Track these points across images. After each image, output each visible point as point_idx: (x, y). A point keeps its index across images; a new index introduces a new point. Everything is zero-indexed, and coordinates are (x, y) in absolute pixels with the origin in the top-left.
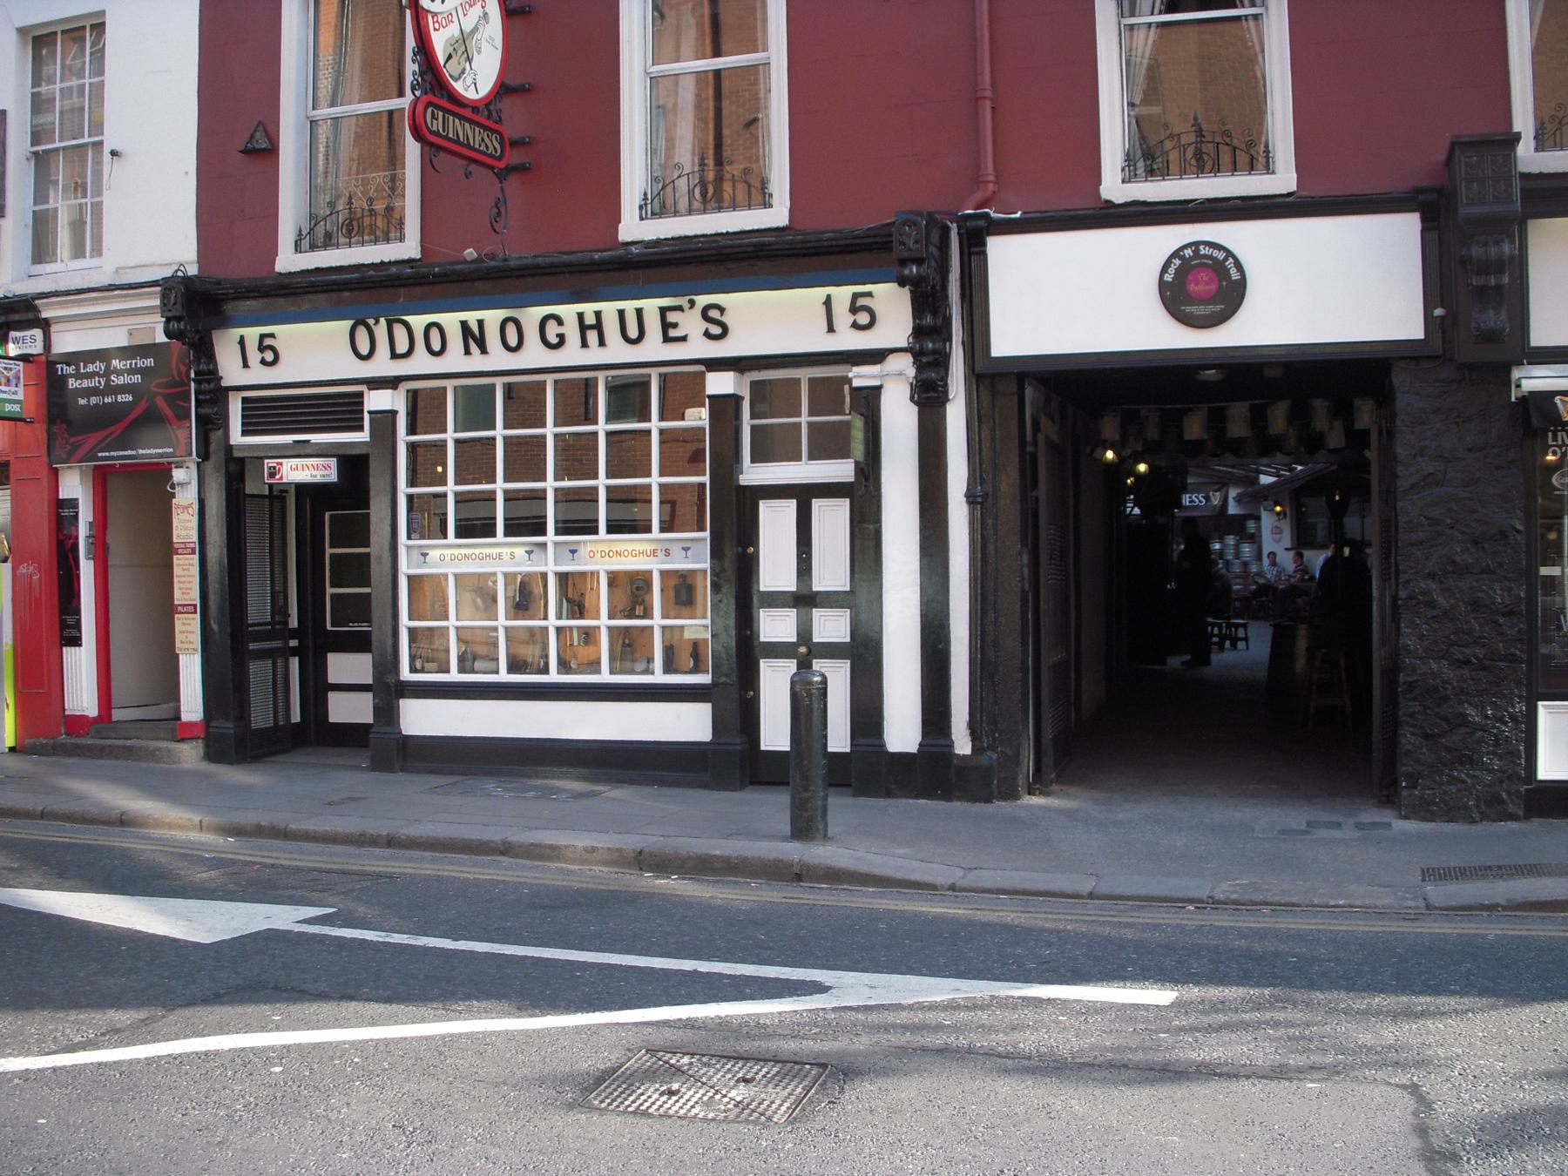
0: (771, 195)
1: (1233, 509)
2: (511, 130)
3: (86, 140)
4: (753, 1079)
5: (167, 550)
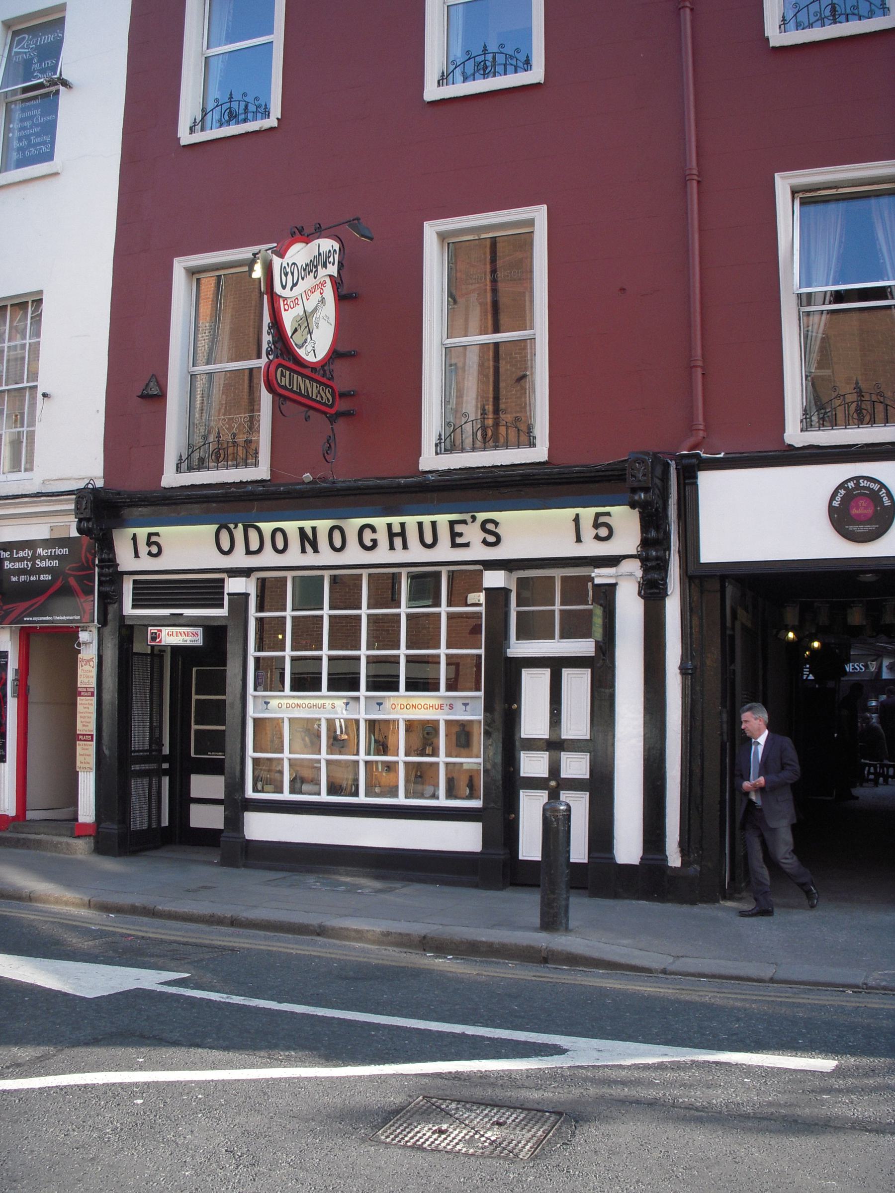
0: (535, 438)
1: (886, 675)
2: (341, 385)
3: (25, 384)
4: (505, 1123)
5: (73, 692)
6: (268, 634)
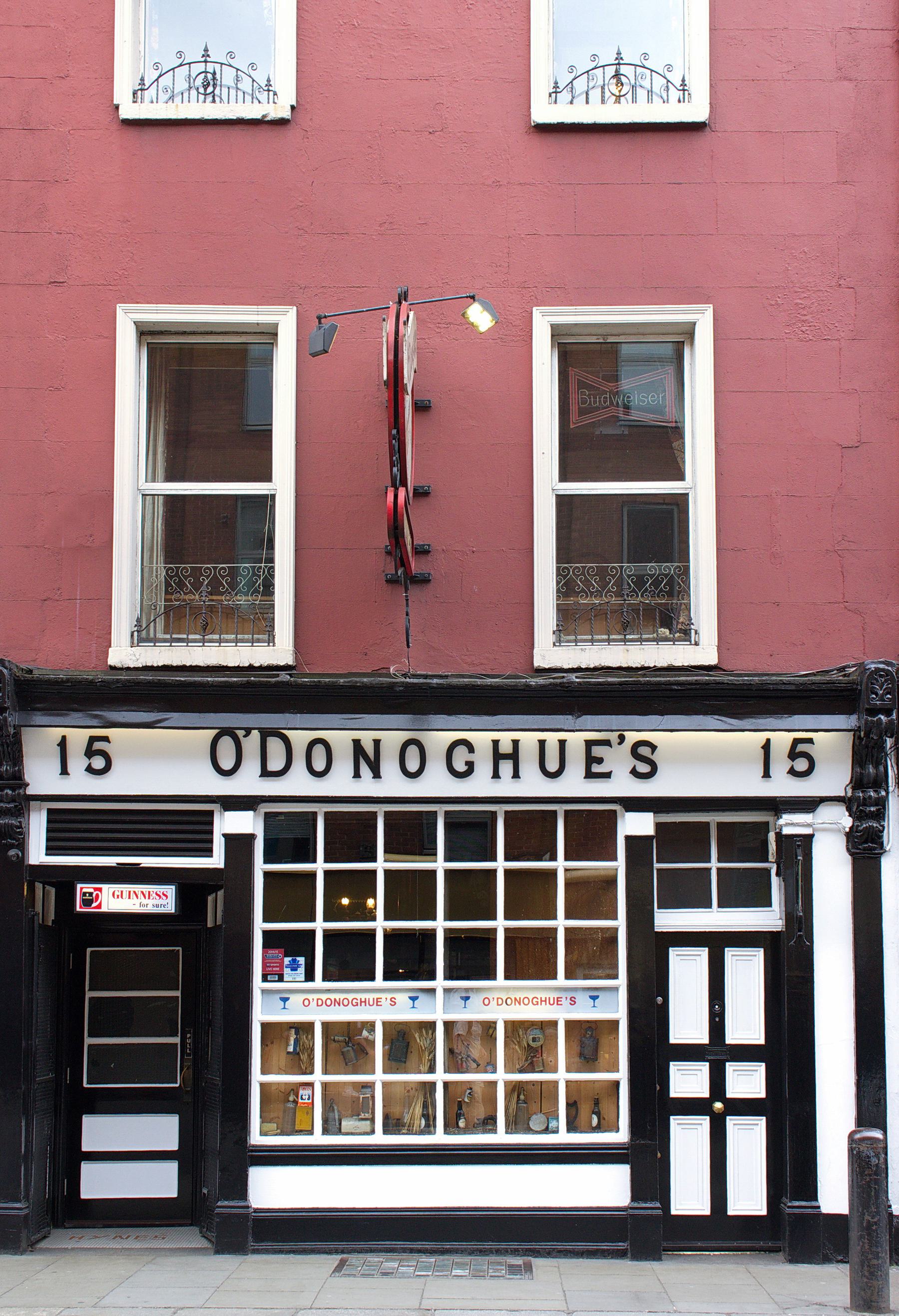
6: (290, 895)
